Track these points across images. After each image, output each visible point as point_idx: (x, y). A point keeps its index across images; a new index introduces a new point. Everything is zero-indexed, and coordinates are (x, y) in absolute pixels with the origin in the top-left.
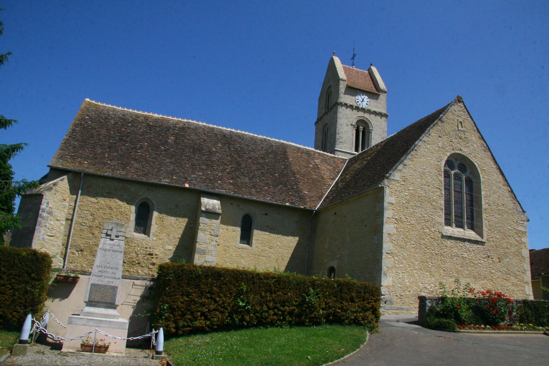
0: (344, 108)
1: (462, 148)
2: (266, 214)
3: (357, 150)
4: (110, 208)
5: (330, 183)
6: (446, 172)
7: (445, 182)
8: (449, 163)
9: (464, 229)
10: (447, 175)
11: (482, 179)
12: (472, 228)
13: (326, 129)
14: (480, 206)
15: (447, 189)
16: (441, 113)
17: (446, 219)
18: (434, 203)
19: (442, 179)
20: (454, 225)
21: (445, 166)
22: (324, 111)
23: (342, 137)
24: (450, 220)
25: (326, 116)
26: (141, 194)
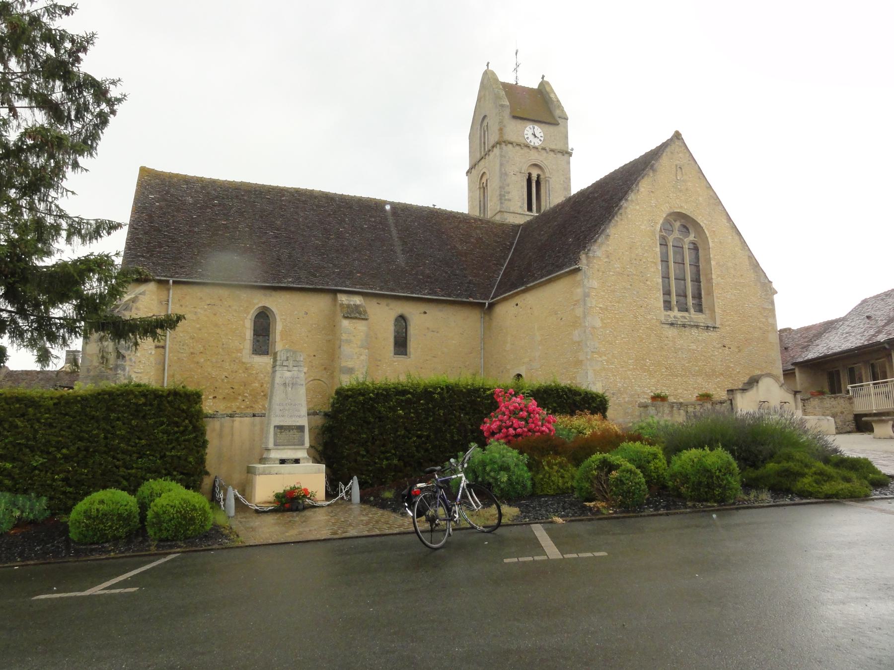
0: (510, 146)
1: (683, 205)
2: (425, 313)
3: (530, 208)
4: (216, 325)
5: (348, 283)
6: (663, 238)
7: (661, 253)
8: (396, 320)
9: (690, 313)
10: (664, 244)
11: (711, 245)
12: (699, 308)
13: (484, 180)
14: (710, 280)
15: (665, 261)
16: (652, 159)
17: (665, 302)
18: (648, 283)
19: (658, 249)
20: (676, 309)
21: (661, 231)
22: (478, 156)
23: (509, 193)
24: (670, 302)
25: (482, 163)
26: (255, 301)
